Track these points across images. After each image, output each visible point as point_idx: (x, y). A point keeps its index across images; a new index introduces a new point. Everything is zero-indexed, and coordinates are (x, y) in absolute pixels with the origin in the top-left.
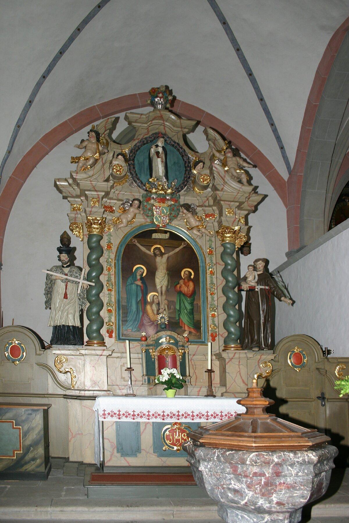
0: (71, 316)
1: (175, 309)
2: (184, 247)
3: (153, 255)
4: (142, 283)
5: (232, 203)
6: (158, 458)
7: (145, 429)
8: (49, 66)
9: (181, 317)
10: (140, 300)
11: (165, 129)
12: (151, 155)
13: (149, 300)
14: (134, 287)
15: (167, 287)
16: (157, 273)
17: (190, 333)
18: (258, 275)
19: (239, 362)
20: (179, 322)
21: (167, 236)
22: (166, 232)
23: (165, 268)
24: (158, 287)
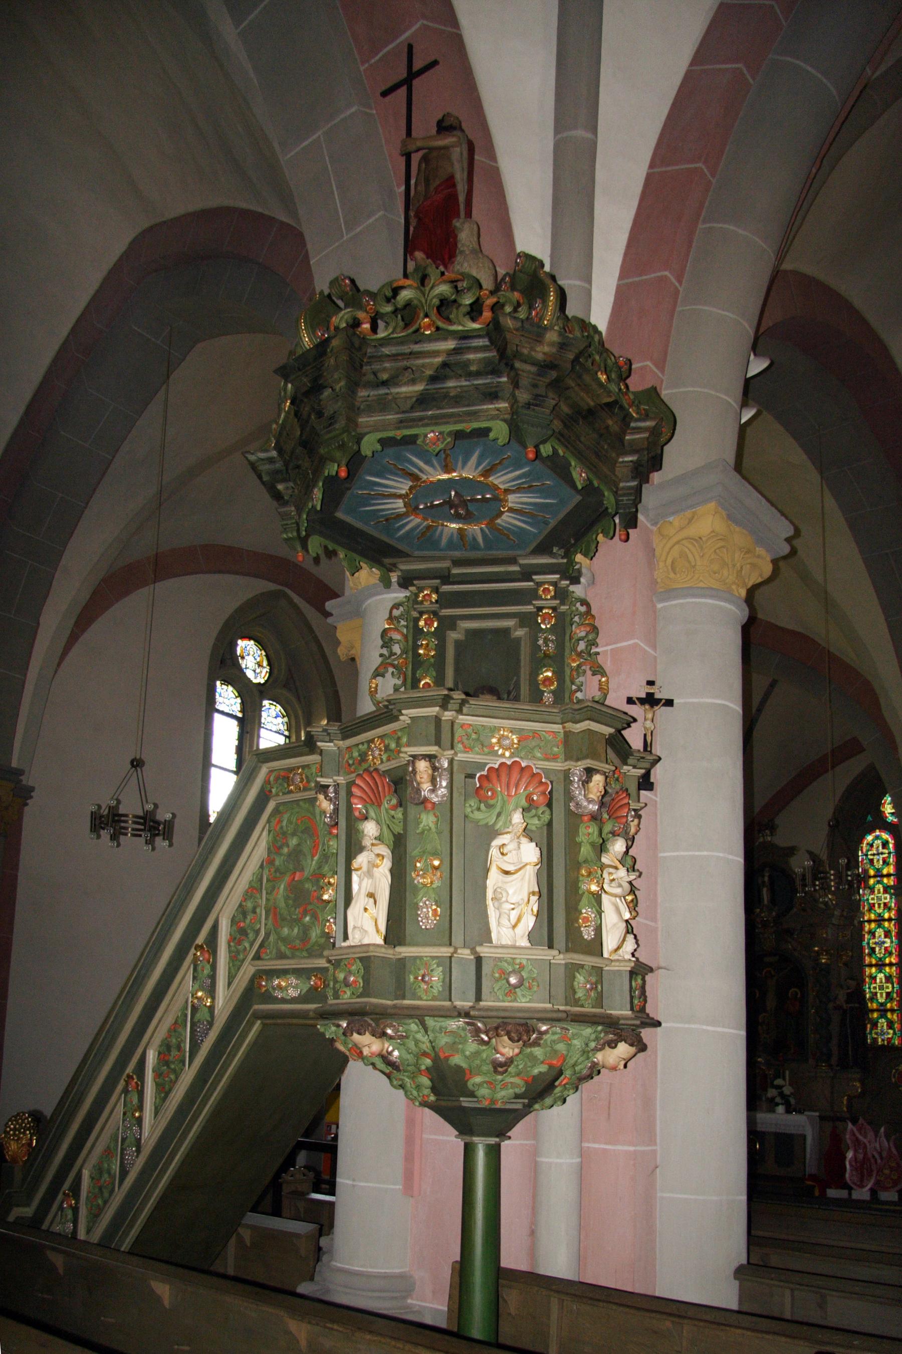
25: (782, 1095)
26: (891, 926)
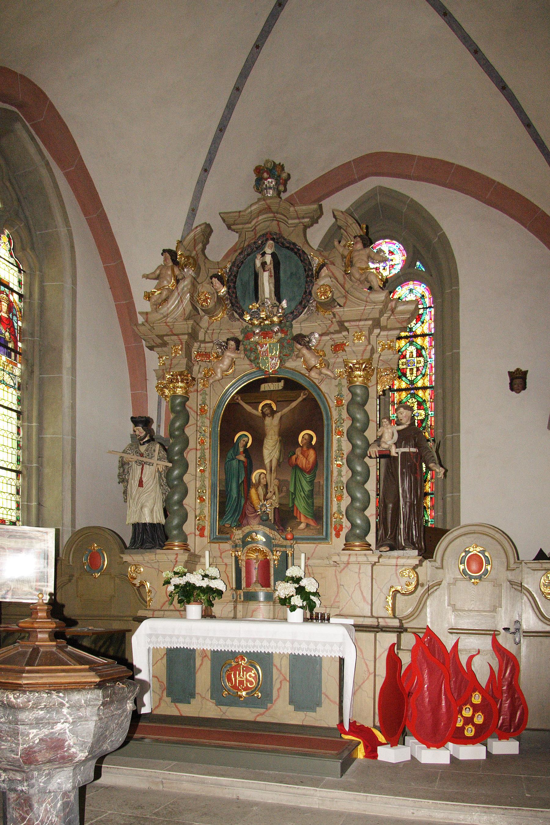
0: (146, 511)
1: (288, 490)
2: (304, 399)
3: (260, 415)
4: (245, 457)
5: (362, 323)
6: (216, 707)
7: (201, 665)
8: (209, 153)
9: (296, 503)
10: (243, 482)
11: (278, 225)
12: (256, 270)
13: (254, 482)
14: (235, 463)
15: (278, 460)
16: (265, 442)
17: (308, 525)
18: (398, 432)
19: (360, 569)
20: (293, 511)
21: (281, 385)
22: (279, 380)
23: (277, 433)
24: (267, 461)
25: (301, 591)
26: (426, 395)
